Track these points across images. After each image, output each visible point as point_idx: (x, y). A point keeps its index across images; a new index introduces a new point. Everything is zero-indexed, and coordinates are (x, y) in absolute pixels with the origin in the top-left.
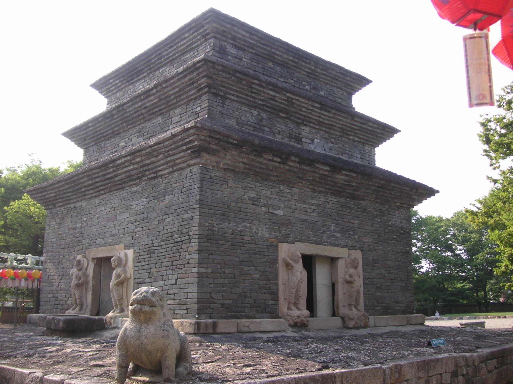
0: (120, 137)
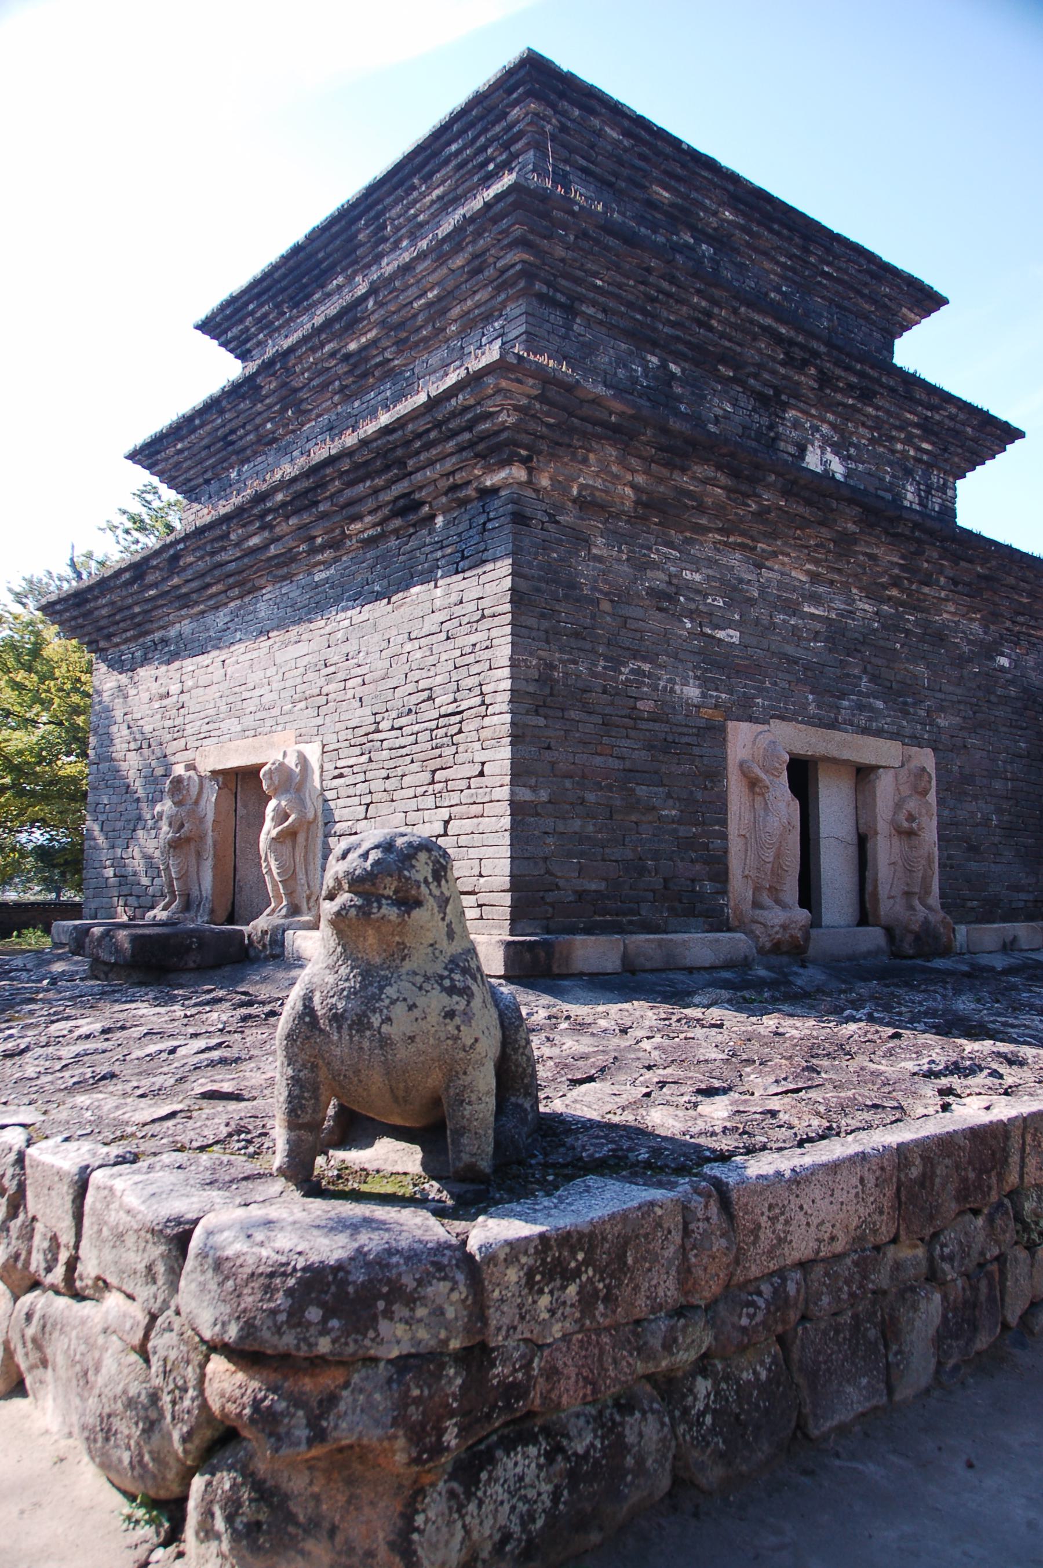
0: (278, 450)
